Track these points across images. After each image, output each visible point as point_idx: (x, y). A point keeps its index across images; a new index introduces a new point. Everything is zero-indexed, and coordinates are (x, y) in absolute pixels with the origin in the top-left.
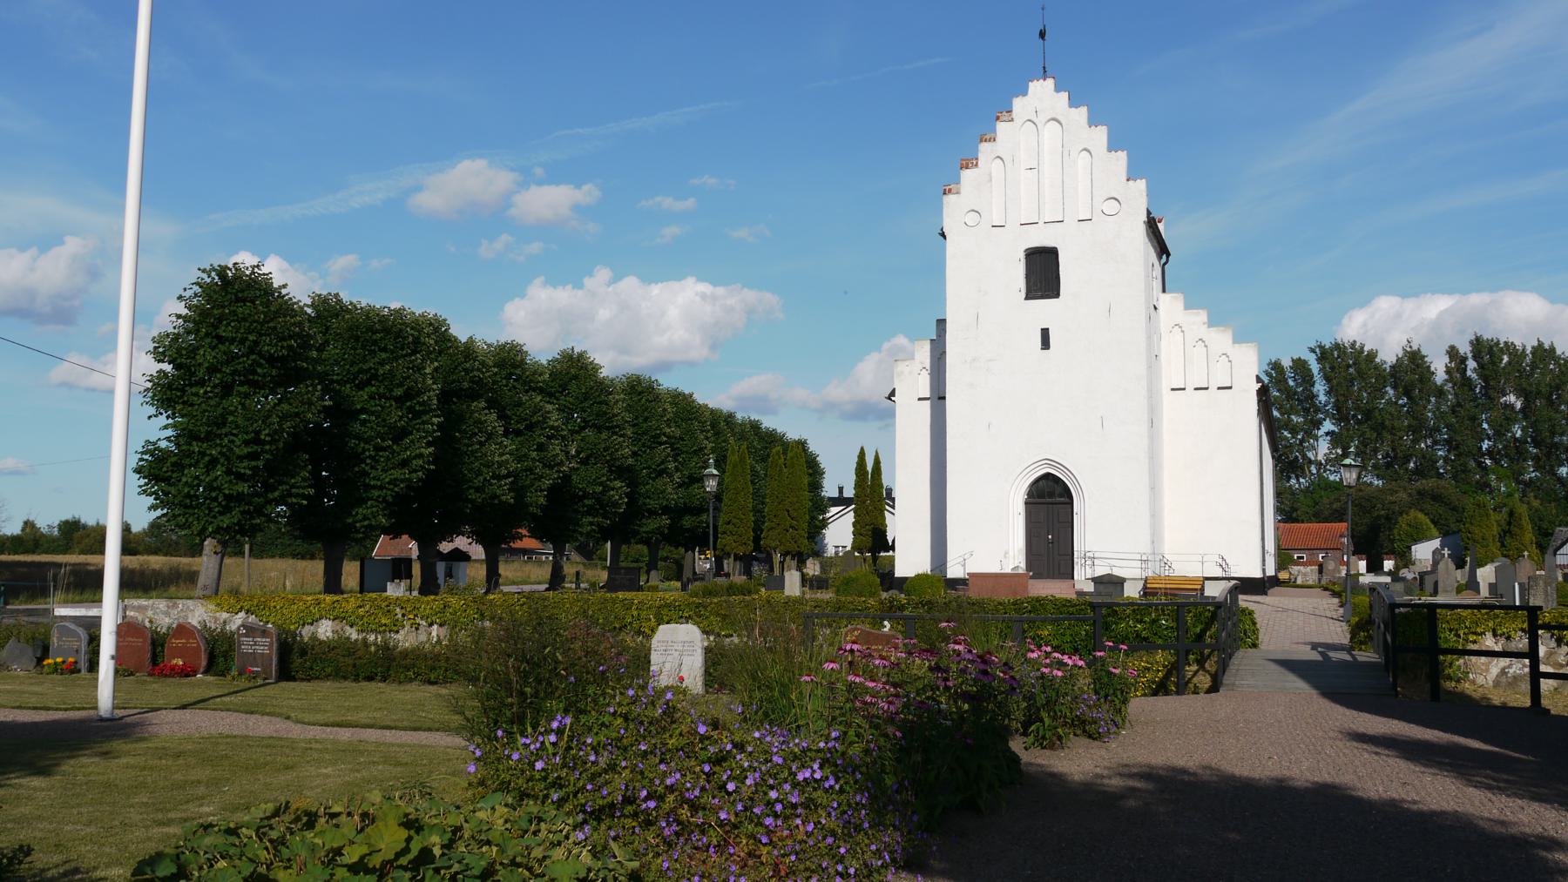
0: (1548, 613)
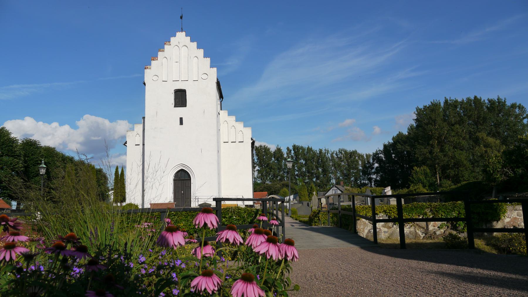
0: (385, 206)
